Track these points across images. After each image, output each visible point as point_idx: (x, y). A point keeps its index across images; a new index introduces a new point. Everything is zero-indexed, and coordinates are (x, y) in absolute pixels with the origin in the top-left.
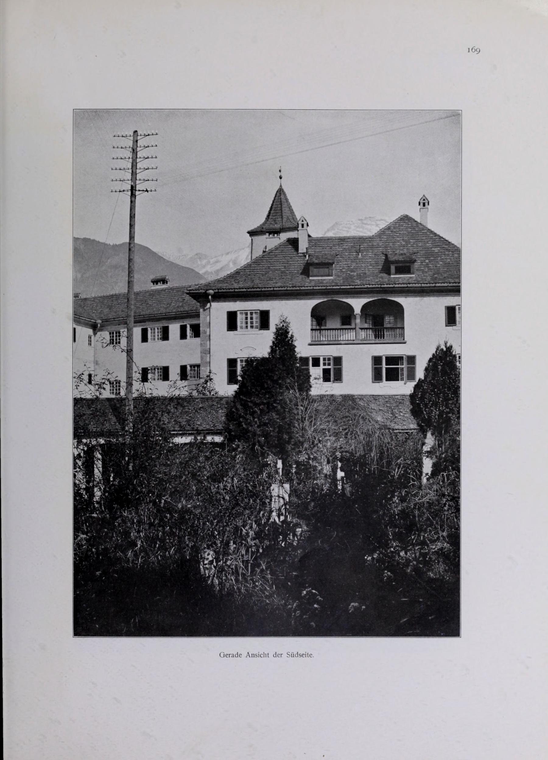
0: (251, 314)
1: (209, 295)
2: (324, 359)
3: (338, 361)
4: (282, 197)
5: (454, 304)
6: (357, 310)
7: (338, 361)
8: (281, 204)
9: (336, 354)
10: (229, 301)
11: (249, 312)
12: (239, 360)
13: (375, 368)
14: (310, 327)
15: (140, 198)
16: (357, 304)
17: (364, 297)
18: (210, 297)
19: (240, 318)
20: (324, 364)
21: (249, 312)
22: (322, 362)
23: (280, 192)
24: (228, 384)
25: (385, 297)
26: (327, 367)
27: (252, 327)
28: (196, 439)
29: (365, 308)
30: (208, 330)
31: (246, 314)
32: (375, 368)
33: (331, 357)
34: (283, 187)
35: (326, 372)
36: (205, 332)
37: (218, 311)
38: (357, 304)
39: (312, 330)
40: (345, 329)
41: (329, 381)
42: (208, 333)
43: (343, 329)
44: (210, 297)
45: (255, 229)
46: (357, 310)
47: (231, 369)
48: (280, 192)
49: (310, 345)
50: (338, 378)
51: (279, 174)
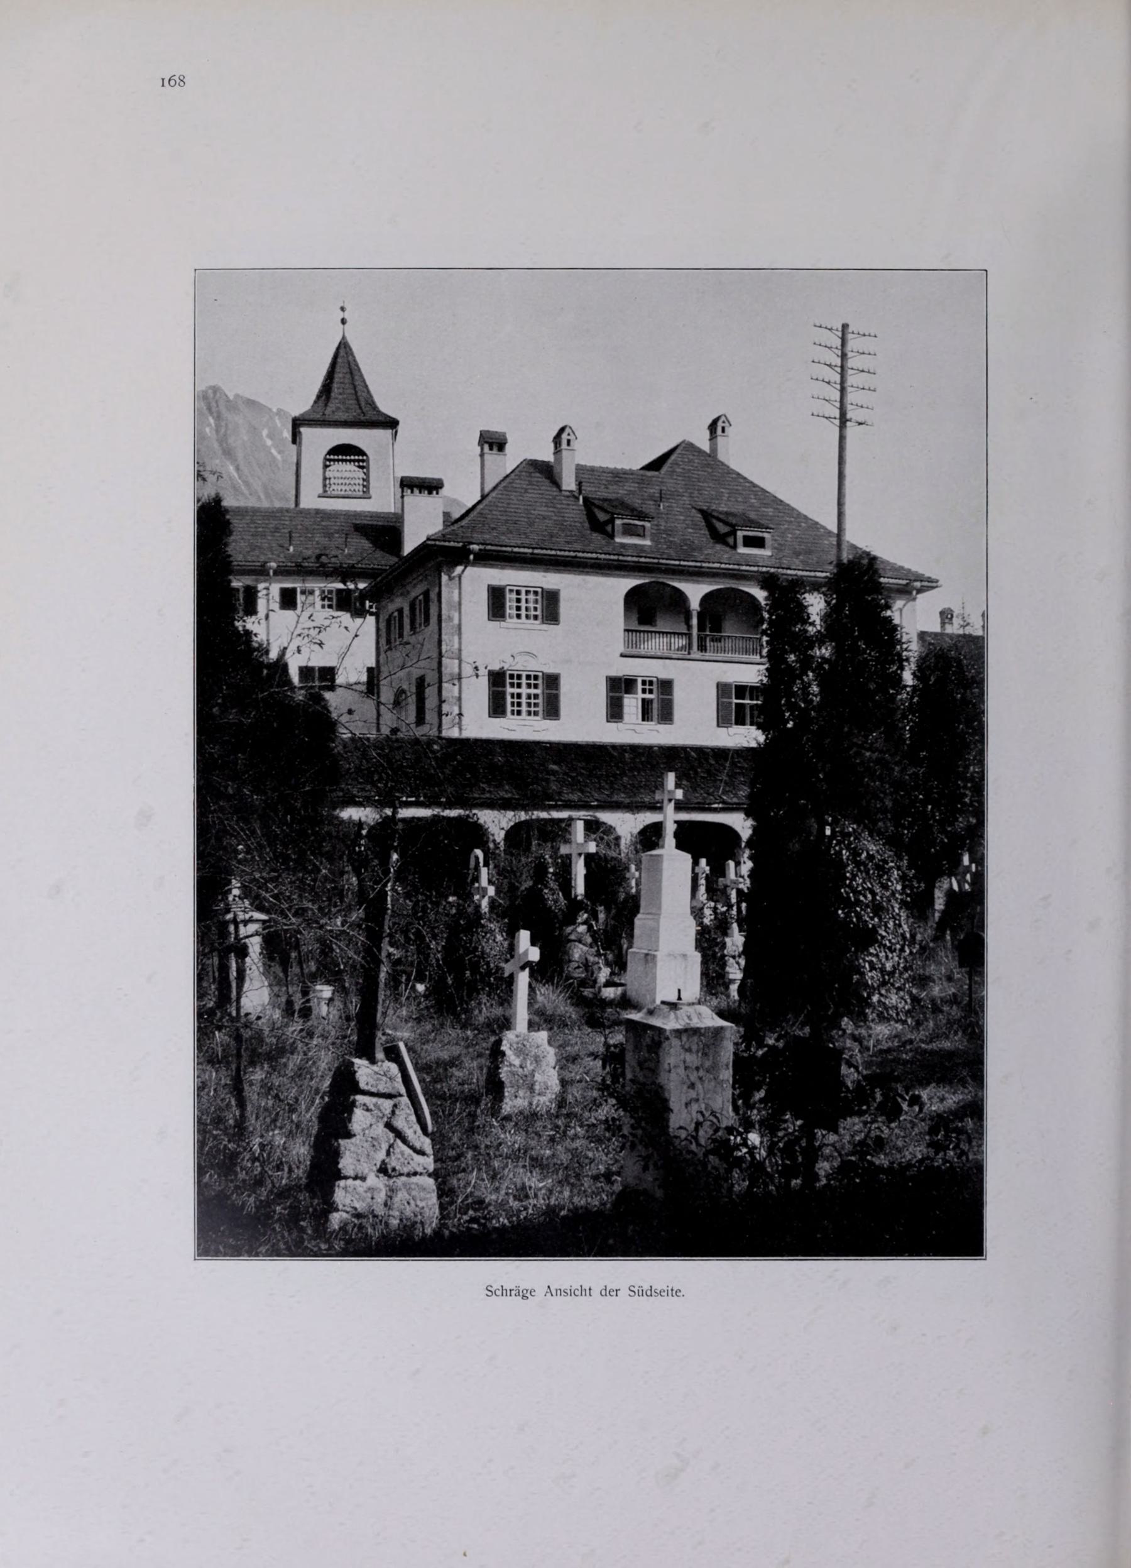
0: (527, 592)
1: (470, 552)
2: (644, 683)
3: (666, 686)
4: (350, 358)
5: (503, 583)
6: (695, 605)
7: (666, 686)
8: (351, 373)
9: (663, 675)
10: (492, 566)
11: (523, 590)
12: (640, 680)
13: (493, 692)
14: (622, 626)
15: (851, 430)
16: (695, 592)
17: (635, 577)
18: (472, 557)
19: (510, 599)
20: (644, 691)
21: (523, 590)
22: (640, 687)
23: (343, 350)
24: (608, 721)
25: (734, 586)
26: (648, 696)
27: (527, 617)
28: (395, 813)
29: (706, 599)
30: (456, 615)
31: (518, 593)
32: (612, 698)
33: (655, 680)
34: (349, 339)
35: (646, 705)
36: (450, 619)
37: (472, 585)
38: (695, 592)
39: (625, 630)
40: (648, 632)
41: (743, 724)
42: (456, 621)
43: (640, 632)
44: (472, 557)
45: (302, 415)
46: (695, 605)
47: (554, 692)
48: (343, 350)
49: (622, 656)
50: (666, 716)
51: (341, 315)
